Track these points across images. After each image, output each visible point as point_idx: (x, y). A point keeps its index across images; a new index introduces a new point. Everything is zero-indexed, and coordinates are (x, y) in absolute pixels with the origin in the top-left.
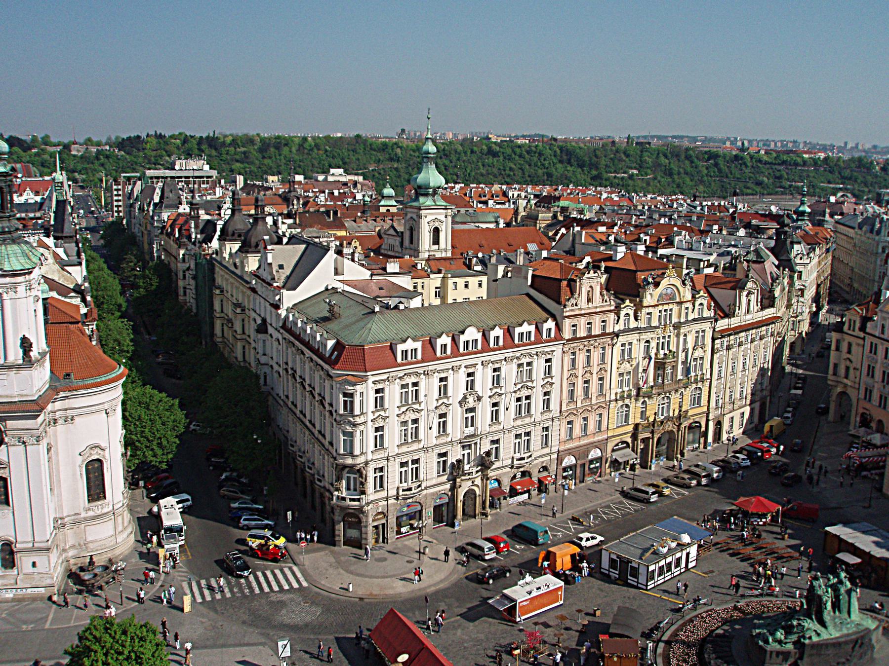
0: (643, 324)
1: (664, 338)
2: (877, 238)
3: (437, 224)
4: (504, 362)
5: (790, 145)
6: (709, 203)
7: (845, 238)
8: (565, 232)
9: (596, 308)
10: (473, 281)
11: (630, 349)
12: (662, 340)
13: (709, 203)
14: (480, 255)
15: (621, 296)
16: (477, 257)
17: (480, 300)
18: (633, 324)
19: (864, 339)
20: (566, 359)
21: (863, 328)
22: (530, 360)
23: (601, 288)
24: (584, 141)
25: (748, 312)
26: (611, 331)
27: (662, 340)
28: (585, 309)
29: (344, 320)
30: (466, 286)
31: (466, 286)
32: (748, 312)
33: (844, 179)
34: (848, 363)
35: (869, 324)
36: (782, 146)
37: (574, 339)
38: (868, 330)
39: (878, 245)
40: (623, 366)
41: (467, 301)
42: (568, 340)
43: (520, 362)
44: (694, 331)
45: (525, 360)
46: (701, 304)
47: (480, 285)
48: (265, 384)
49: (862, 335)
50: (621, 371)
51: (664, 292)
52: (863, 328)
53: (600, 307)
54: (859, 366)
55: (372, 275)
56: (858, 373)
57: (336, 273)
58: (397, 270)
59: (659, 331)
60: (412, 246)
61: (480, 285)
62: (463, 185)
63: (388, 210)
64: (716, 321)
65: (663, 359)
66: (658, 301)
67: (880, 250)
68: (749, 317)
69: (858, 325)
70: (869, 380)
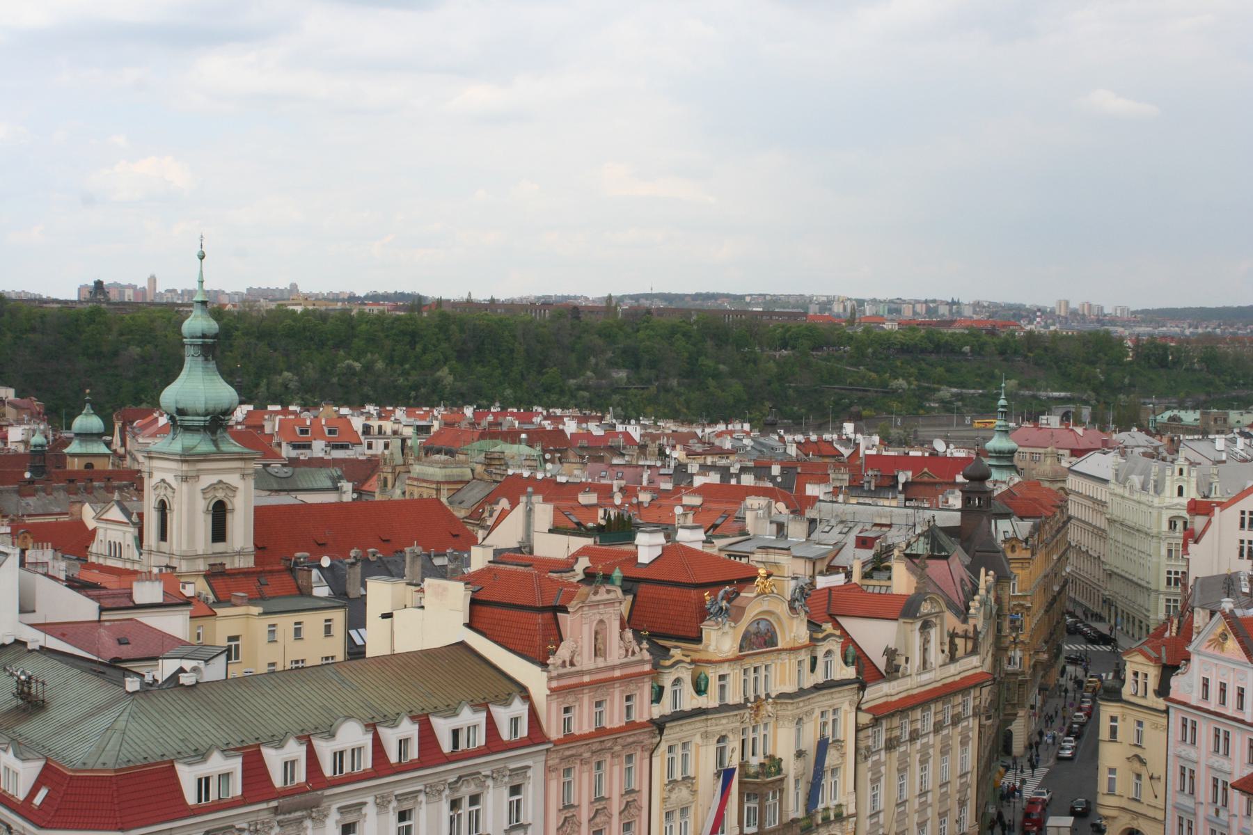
0: (710, 700)
1: (754, 729)
2: (1156, 501)
3: (220, 495)
4: (422, 797)
5: (944, 310)
6: (800, 438)
7: (1089, 503)
8: (508, 507)
9: (613, 668)
10: (313, 622)
11: (685, 756)
12: (751, 735)
13: (800, 438)
14: (326, 562)
15: (662, 642)
16: (320, 567)
17: (328, 661)
18: (690, 700)
19: (1167, 711)
20: (553, 785)
21: (1163, 690)
22: (477, 791)
23: (623, 627)
24: (586, 299)
25: (925, 667)
26: (646, 718)
27: (751, 735)
28: (590, 672)
29: (59, 714)
30: (298, 633)
31: (298, 633)
32: (925, 667)
33: (1067, 379)
34: (1136, 765)
35: (1174, 681)
36: (929, 310)
37: (569, 738)
38: (1172, 695)
39: (1160, 515)
40: (673, 796)
41: (299, 669)
42: (556, 743)
43: (457, 795)
44: (817, 712)
45: (466, 791)
46: (829, 653)
47: (328, 630)
48: (1111, 792)
49: (1161, 703)
50: (669, 807)
51: (753, 629)
52: (1163, 690)
53: (622, 666)
54: (1159, 771)
55: (102, 610)
56: (1160, 788)
57: (23, 610)
58: (159, 599)
59: (747, 713)
60: (164, 546)
61: (328, 630)
62: (251, 408)
63: (89, 466)
64: (862, 687)
65: (757, 775)
66: (741, 648)
67: (1165, 526)
68: (926, 677)
69: (1153, 683)
70: (1187, 802)
